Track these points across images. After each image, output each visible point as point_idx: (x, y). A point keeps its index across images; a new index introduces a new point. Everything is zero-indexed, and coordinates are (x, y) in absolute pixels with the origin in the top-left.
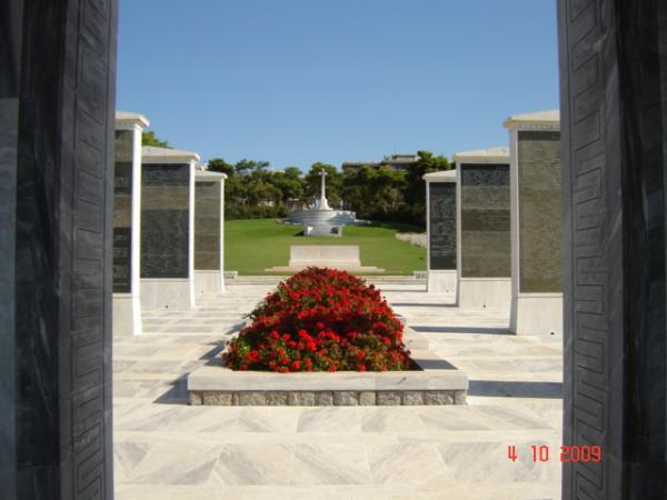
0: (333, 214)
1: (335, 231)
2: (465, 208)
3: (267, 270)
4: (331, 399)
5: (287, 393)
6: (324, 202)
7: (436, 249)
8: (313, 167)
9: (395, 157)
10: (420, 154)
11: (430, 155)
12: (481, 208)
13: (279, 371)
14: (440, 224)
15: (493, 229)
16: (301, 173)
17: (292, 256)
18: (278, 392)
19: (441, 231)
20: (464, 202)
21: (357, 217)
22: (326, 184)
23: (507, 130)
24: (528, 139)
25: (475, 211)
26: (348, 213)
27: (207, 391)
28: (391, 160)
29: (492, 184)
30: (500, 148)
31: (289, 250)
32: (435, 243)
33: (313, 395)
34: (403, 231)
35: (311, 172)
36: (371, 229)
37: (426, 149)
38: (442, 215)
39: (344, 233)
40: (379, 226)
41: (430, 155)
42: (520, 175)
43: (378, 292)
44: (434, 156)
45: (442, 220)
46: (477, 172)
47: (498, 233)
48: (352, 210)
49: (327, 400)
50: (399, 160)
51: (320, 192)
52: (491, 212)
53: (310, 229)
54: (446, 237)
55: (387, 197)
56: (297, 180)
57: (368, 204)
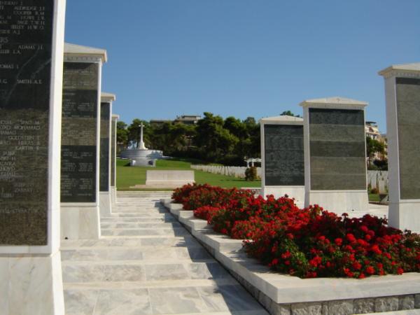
0: (150, 152)
1: (151, 163)
2: (312, 140)
3: (131, 187)
4: (413, 302)
5: (374, 299)
6: (143, 144)
7: (269, 171)
8: (134, 121)
9: (184, 117)
10: (205, 114)
11: (212, 115)
12: (324, 140)
13: (354, 277)
14: (272, 153)
15: (331, 155)
16: (126, 125)
17: (148, 178)
18: (366, 299)
19: (272, 159)
20: (311, 135)
21: (164, 155)
22: (144, 133)
23: (382, 77)
24: (402, 83)
25: (319, 142)
26: (159, 151)
27: (296, 304)
28: (181, 119)
29: (330, 123)
30: (336, 98)
31: (146, 174)
32: (269, 167)
33: (397, 300)
34: (195, 163)
35: (132, 125)
36: (173, 162)
37: (209, 111)
38: (272, 148)
39: (157, 164)
40: (179, 160)
41: (212, 115)
42: (398, 111)
43: (292, 201)
44: (214, 116)
45: (271, 151)
46: (320, 114)
47: (335, 158)
48: (161, 150)
49: (410, 304)
50: (186, 119)
51: (139, 138)
52: (330, 143)
53: (134, 162)
54: (275, 163)
55: (182, 142)
56: (123, 130)
57: (168, 147)
